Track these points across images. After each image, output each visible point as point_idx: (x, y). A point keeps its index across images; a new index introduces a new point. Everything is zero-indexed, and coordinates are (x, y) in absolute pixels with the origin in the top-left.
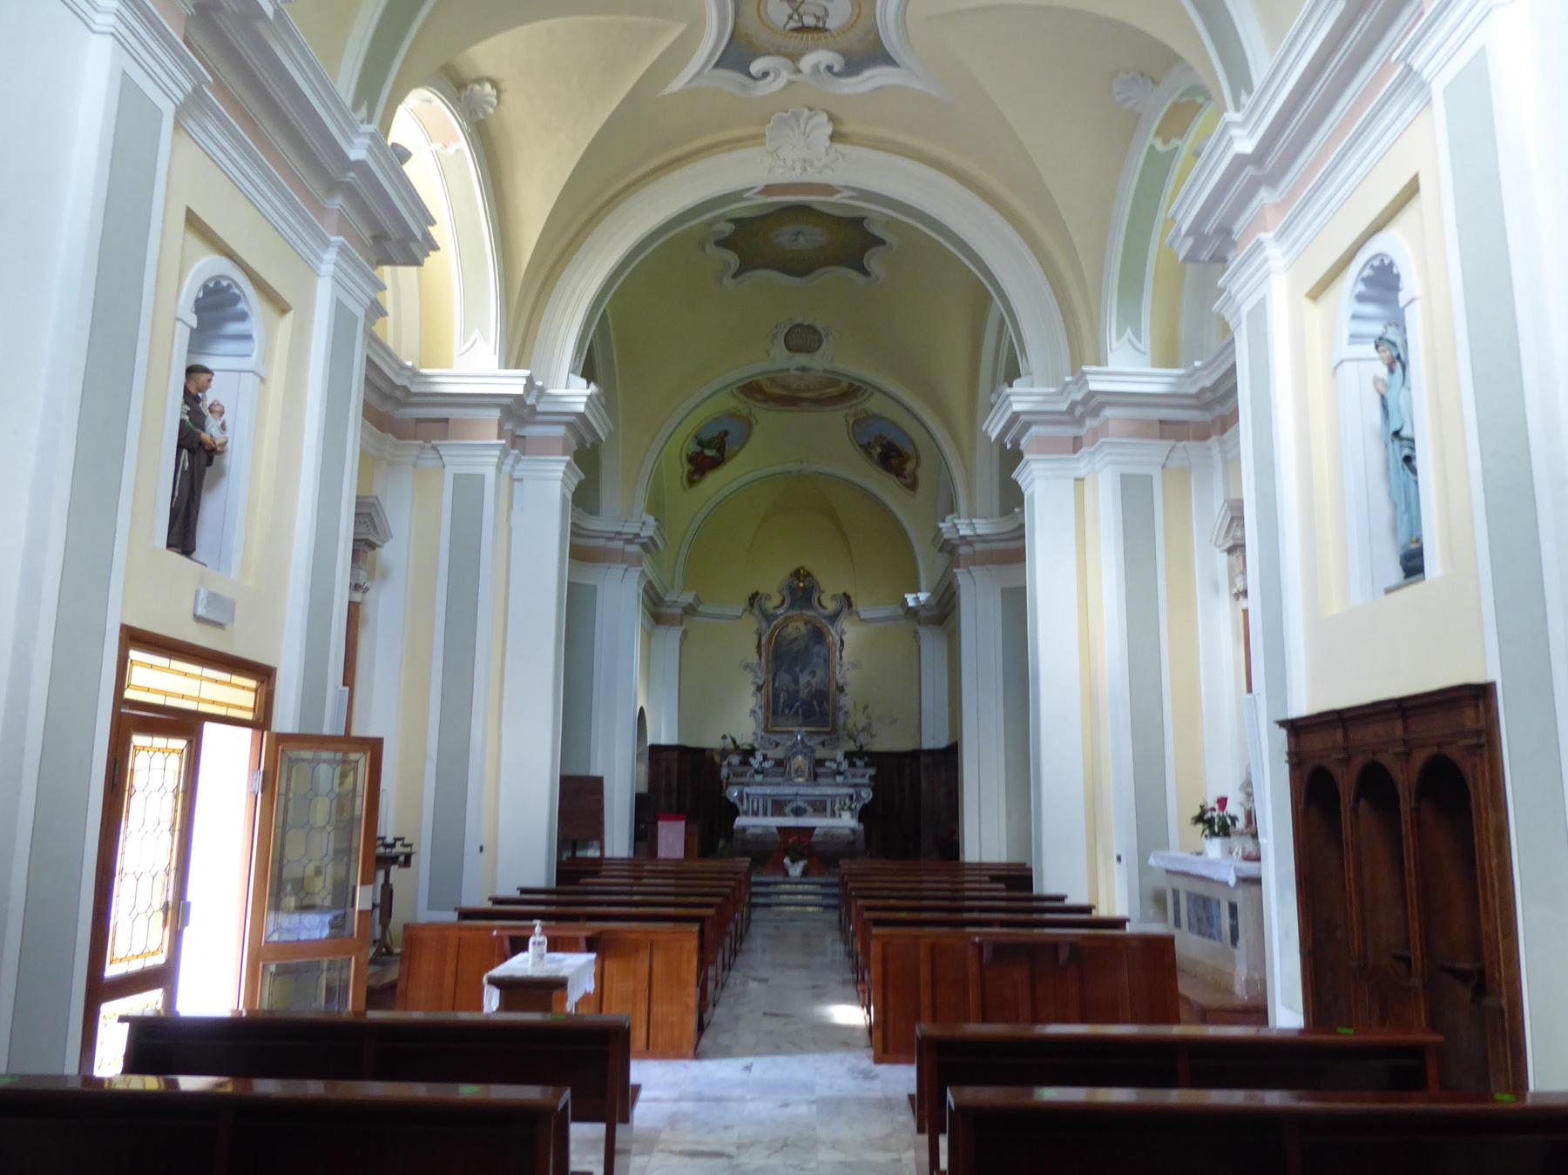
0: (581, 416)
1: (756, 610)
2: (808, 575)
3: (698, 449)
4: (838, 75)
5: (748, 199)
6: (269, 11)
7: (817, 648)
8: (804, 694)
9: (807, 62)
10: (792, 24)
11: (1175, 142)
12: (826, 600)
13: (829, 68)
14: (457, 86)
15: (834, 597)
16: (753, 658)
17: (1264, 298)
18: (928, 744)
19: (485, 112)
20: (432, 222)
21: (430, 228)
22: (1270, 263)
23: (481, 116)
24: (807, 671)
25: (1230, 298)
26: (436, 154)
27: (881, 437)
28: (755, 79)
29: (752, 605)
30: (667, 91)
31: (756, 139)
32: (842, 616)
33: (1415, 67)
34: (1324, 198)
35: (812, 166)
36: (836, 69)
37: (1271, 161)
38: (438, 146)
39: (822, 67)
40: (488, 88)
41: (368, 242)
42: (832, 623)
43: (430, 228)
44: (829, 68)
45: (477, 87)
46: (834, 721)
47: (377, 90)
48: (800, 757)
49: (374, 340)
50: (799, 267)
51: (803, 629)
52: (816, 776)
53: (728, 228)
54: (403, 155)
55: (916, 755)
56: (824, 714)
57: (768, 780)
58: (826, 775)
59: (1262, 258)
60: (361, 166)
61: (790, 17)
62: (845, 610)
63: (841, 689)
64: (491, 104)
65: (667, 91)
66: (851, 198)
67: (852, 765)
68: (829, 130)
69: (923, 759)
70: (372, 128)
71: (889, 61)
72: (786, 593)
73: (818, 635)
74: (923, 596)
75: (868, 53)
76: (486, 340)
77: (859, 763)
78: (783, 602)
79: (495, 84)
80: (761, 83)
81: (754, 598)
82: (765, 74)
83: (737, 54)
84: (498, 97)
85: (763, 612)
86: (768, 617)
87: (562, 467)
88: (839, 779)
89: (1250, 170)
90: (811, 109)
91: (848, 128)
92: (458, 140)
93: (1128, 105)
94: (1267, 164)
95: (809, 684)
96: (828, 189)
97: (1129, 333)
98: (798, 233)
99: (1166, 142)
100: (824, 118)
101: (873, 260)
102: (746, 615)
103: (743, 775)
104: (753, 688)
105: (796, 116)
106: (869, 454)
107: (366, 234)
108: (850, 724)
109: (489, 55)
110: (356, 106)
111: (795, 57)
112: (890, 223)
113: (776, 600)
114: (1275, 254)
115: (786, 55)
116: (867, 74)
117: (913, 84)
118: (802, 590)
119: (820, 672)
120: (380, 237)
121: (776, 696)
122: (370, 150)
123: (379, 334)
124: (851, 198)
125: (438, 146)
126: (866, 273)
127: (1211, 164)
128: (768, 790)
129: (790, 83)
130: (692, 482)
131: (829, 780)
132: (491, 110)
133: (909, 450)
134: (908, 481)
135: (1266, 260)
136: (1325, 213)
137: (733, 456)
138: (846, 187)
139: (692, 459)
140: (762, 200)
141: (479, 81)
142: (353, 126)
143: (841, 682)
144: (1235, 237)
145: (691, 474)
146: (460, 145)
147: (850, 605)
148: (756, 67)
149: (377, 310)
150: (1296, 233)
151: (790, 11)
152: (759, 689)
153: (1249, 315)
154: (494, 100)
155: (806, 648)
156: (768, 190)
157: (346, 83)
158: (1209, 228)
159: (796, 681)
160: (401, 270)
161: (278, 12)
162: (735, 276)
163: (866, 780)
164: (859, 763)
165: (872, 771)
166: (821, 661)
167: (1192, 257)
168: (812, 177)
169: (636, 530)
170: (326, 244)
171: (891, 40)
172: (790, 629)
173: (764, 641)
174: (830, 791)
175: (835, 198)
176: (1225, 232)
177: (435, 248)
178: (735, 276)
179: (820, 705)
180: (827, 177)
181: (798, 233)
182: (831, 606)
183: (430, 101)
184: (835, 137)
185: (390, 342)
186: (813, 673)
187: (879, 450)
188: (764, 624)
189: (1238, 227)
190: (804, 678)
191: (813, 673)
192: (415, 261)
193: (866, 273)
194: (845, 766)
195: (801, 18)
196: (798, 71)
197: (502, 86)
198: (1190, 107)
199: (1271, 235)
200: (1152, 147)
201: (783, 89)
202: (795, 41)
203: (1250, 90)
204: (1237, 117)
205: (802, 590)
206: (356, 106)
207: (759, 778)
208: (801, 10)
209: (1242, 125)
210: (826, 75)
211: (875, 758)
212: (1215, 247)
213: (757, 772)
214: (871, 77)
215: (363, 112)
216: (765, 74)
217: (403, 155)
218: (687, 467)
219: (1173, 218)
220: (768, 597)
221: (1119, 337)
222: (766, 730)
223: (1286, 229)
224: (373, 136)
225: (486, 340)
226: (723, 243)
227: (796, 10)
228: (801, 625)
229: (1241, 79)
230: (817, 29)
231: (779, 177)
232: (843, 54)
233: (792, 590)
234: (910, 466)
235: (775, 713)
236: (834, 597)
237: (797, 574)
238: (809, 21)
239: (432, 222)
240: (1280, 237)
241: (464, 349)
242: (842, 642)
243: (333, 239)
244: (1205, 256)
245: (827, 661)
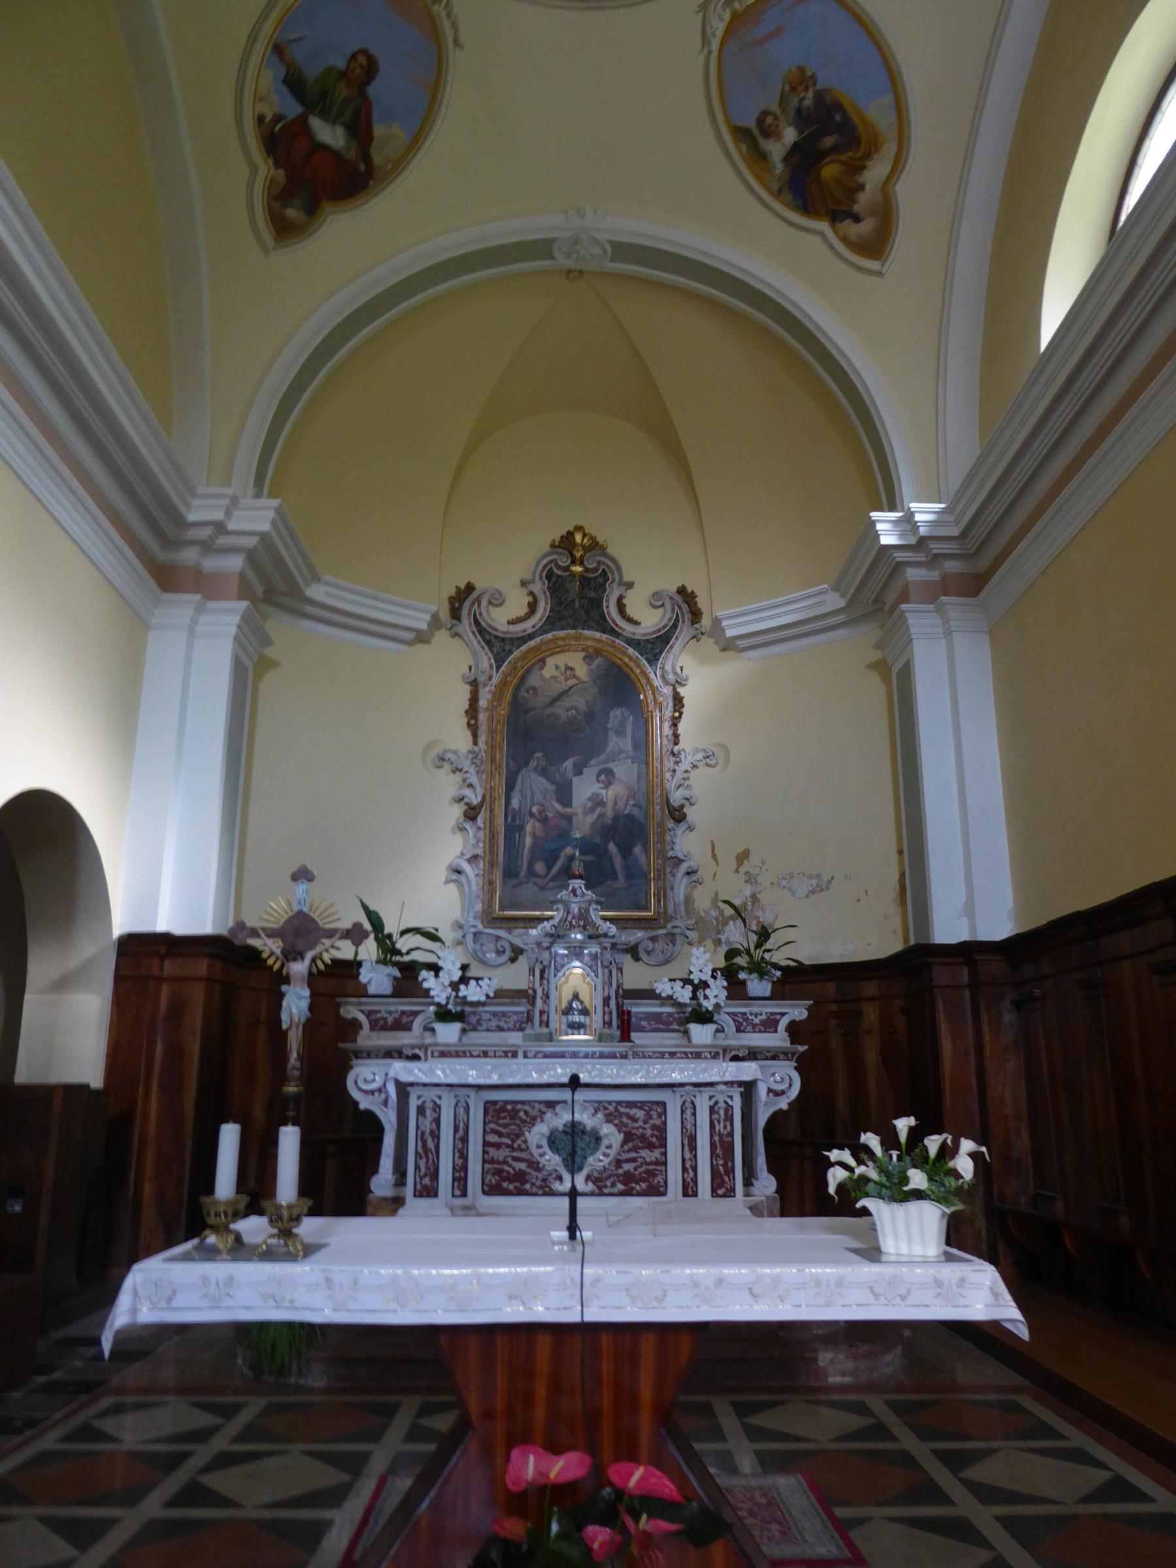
0: (264, 537)
1: (466, 626)
2: (595, 546)
3: (294, 109)
7: (616, 714)
8: (583, 826)
12: (636, 604)
15: (656, 599)
16: (459, 740)
18: (948, 929)
24: (590, 772)
27: (801, 80)
29: (455, 614)
32: (677, 643)
42: (653, 660)
46: (662, 894)
48: (577, 969)
51: (582, 670)
52: (626, 1027)
55: (919, 963)
56: (634, 873)
57: (477, 1038)
58: (659, 1023)
62: (685, 631)
63: (678, 815)
67: (736, 990)
69: (940, 975)
72: (538, 588)
73: (619, 687)
74: (925, 512)
77: (757, 986)
78: (533, 607)
81: (461, 599)
85: (481, 630)
86: (499, 645)
87: (236, 619)
88: (701, 1034)
95: (597, 801)
102: (442, 636)
103: (401, 1025)
104: (457, 811)
106: (758, 157)
108: (702, 900)
113: (517, 604)
118: (578, 588)
119: (625, 771)
121: (514, 829)
128: (471, 1072)
130: (285, 230)
131: (669, 1040)
133: (876, 112)
134: (866, 227)
137: (401, 162)
139: (281, 140)
143: (676, 797)
145: (279, 197)
147: (696, 615)
152: (471, 814)
155: (590, 716)
159: (564, 794)
163: (778, 1039)
164: (757, 986)
165: (797, 1011)
166: (627, 744)
169: (219, 516)
172: (549, 671)
173: (482, 703)
174: (678, 1072)
179: (626, 852)
182: (649, 621)
186: (608, 776)
187: (790, 135)
188: (486, 660)
190: (585, 788)
191: (608, 776)
194: (716, 992)
205: (578, 588)
207: (448, 1033)
211: (795, 979)
213: (444, 1015)
218: (265, 167)
220: (497, 600)
222: (492, 920)
228: (575, 660)
233: (556, 582)
234: (874, 175)
235: (510, 873)
236: (656, 599)
237: (566, 543)
242: (678, 701)
245: (643, 746)
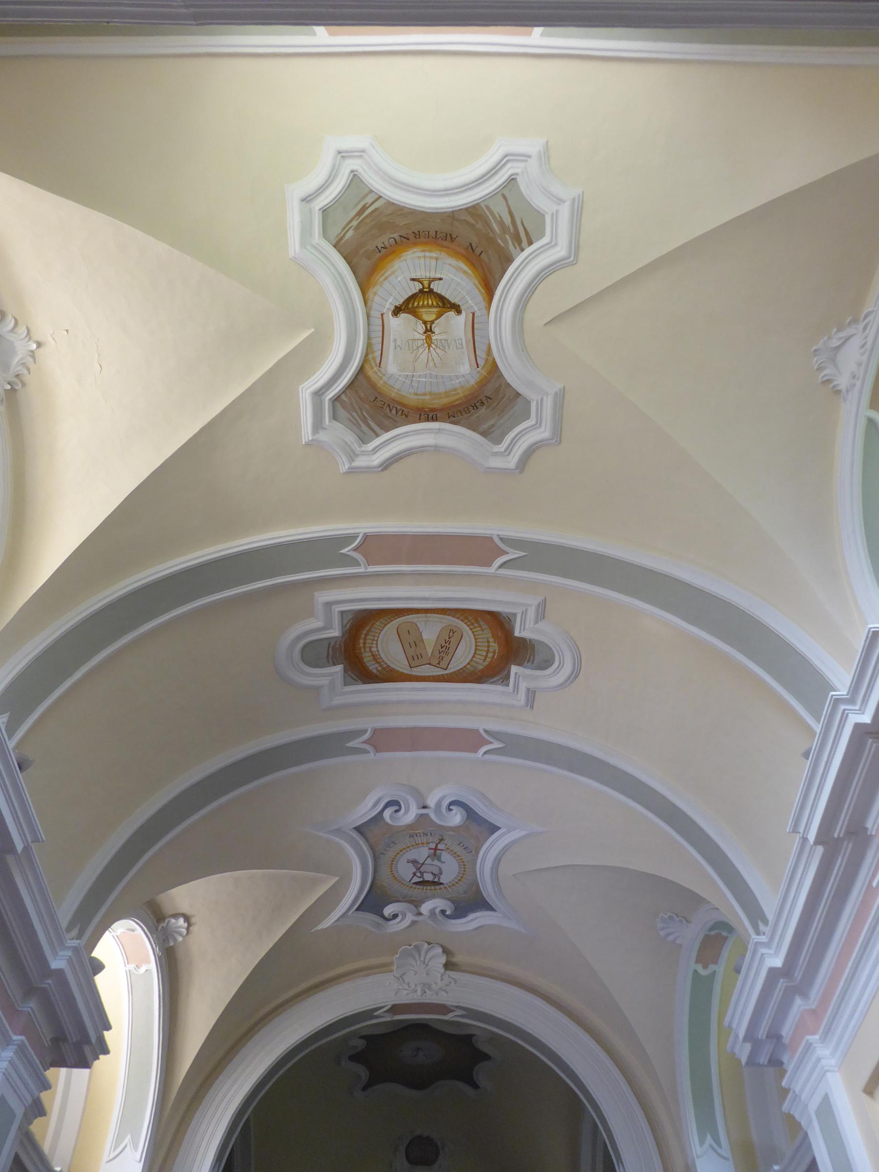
4: (450, 917)
5: (378, 1017)
6: (19, 846)
9: (425, 908)
10: (416, 880)
11: (712, 967)
13: (443, 912)
14: (156, 920)
17: (827, 1095)
19: (175, 940)
20: (108, 1027)
21: (105, 1033)
22: (823, 1062)
23: (171, 944)
25: (796, 1097)
26: (129, 974)
28: (387, 920)
30: (320, 927)
31: (384, 968)
33: (797, 1092)
34: (848, 1012)
35: (430, 988)
36: (448, 913)
37: (798, 974)
38: (132, 967)
39: (438, 911)
40: (181, 921)
41: (47, 1042)
43: (105, 1033)
44: (443, 912)
45: (173, 921)
47: (91, 920)
49: (29, 1141)
50: (419, 1080)
53: (360, 1044)
54: (98, 967)
59: (813, 1059)
60: (60, 972)
61: (414, 874)
64: (180, 934)
65: (320, 927)
66: (462, 1016)
68: (443, 960)
70: (75, 943)
71: (490, 908)
75: (471, 901)
76: (136, 1148)
79: (187, 919)
80: (391, 923)
82: (395, 916)
83: (373, 901)
84: (188, 929)
89: (782, 983)
90: (429, 944)
91: (458, 959)
92: (149, 962)
93: (671, 938)
94: (792, 979)
96: (443, 1009)
97: (709, 1140)
98: (418, 1049)
99: (705, 967)
100: (440, 950)
101: (481, 1073)
105: (418, 948)
107: (47, 1034)
109: (184, 897)
110: (69, 929)
111: (417, 903)
112: (493, 1038)
114: (825, 1054)
115: (410, 902)
116: (471, 916)
117: (506, 924)
120: (59, 1039)
122: (70, 961)
123: (37, 1137)
124: (462, 1016)
125: (132, 967)
126: (476, 1086)
127: (745, 993)
129: (414, 923)
132: (180, 939)
135: (819, 1060)
136: (857, 1015)
138: (458, 1007)
140: (388, 1018)
141: (176, 916)
142: (61, 941)
144: (786, 1041)
146: (150, 968)
148: (388, 911)
149: (38, 1110)
150: (839, 1032)
151: (415, 870)
153: (818, 1113)
154: (184, 931)
156: (395, 1009)
157: (65, 912)
158: (762, 1033)
160: (76, 1071)
161: (26, 849)
162: (364, 1089)
167: (752, 1061)
168: (430, 998)
170: (8, 1042)
171: (488, 891)
175: (448, 1017)
176: (775, 1036)
177: (105, 1051)
178: (364, 1089)
180: (443, 999)
181: (418, 1049)
183: (133, 930)
184: (448, 966)
185: (46, 1148)
189: (786, 1031)
192: (84, 1063)
193: (476, 1086)
195: (422, 874)
196: (420, 914)
197: (193, 920)
198: (717, 939)
199: (817, 1037)
200: (696, 971)
201: (409, 926)
202: (418, 891)
203: (766, 922)
204: (763, 939)
206: (69, 929)
208: (422, 869)
209: (768, 945)
210: (440, 918)
212: (771, 1056)
214: (475, 919)
215: (75, 932)
216: (395, 916)
217: (98, 967)
219: (730, 1027)
221: (702, 1143)
223: (828, 1031)
224: (76, 950)
225: (136, 1148)
226: (355, 1058)
227: (418, 869)
229: (756, 915)
230: (434, 883)
231: (405, 998)
232: (453, 902)
238: (428, 877)
239: (108, 1027)
240: (824, 1039)
241: (112, 1155)
243: (15, 1037)
244: (763, 1059)
